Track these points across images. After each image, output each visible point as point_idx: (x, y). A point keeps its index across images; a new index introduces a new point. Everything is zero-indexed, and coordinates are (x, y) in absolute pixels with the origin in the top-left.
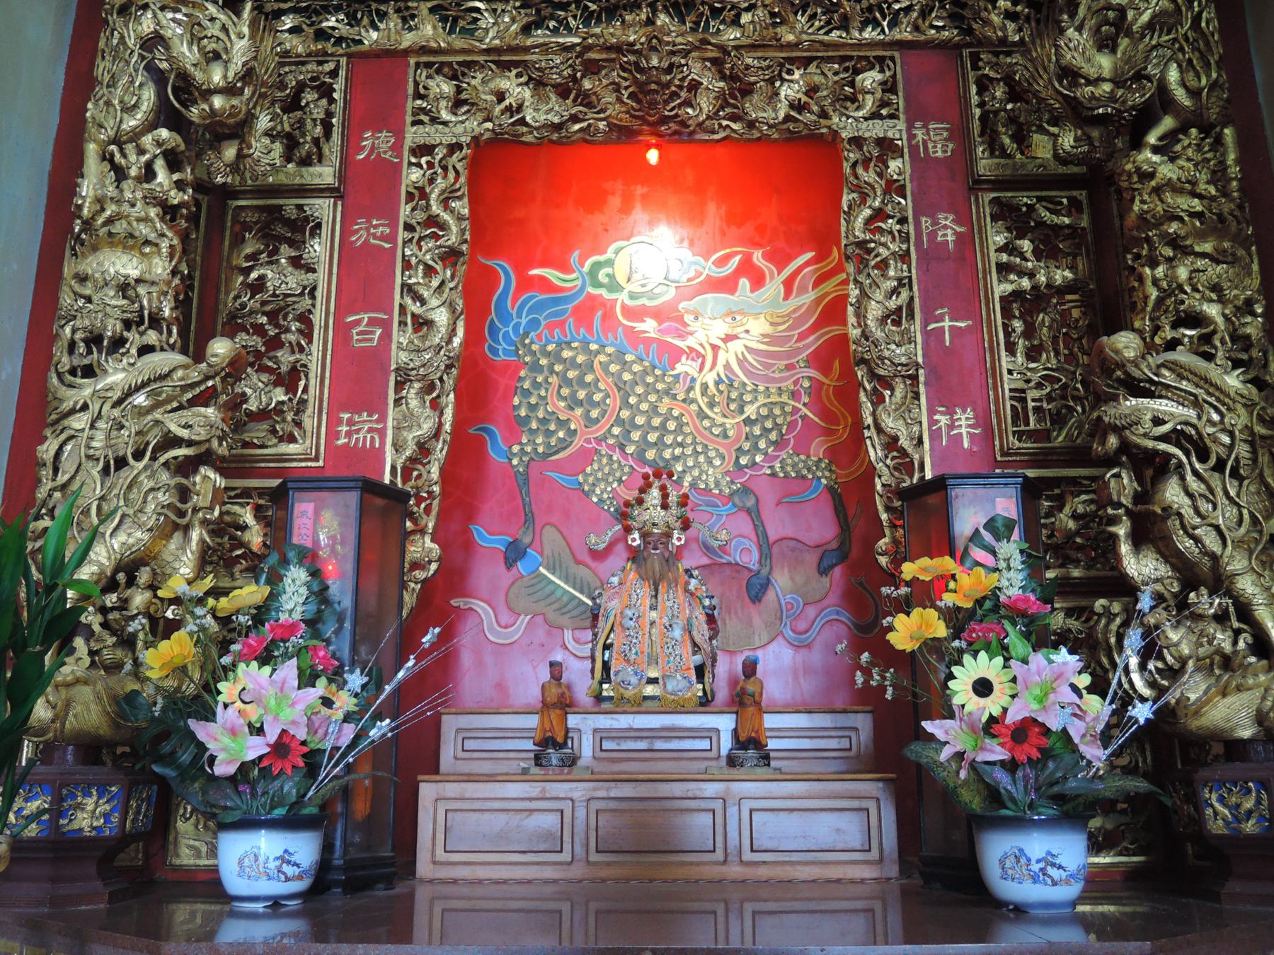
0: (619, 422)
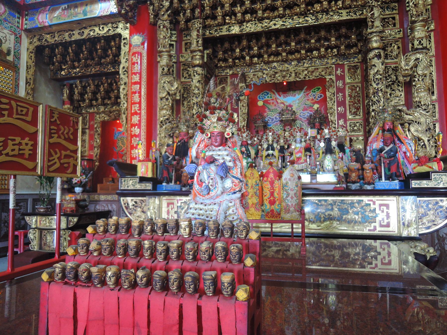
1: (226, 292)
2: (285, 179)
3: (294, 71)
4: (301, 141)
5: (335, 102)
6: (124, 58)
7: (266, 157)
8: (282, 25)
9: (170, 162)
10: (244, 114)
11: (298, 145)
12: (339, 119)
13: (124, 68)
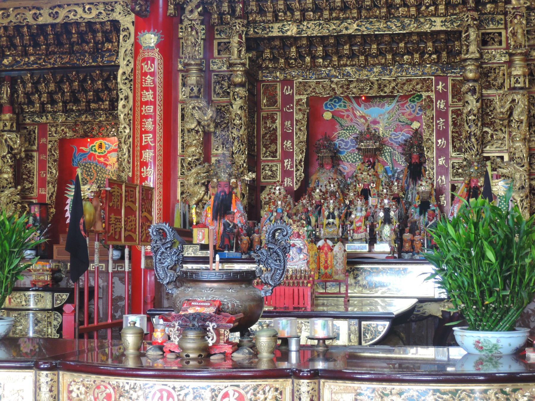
0: (96, 179)
1: (305, 285)
2: (336, 251)
3: (377, 80)
4: (361, 210)
5: (433, 131)
6: (124, 59)
7: (327, 225)
8: (356, 29)
9: (231, 230)
10: (302, 142)
11: (359, 214)
12: (439, 156)
13: (124, 73)
